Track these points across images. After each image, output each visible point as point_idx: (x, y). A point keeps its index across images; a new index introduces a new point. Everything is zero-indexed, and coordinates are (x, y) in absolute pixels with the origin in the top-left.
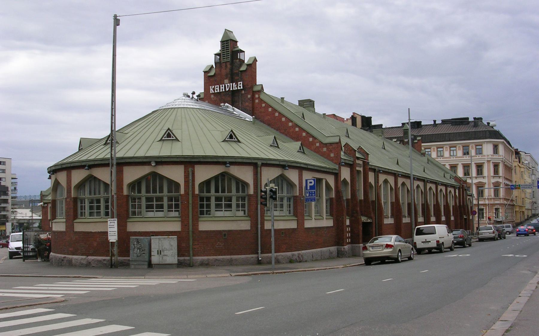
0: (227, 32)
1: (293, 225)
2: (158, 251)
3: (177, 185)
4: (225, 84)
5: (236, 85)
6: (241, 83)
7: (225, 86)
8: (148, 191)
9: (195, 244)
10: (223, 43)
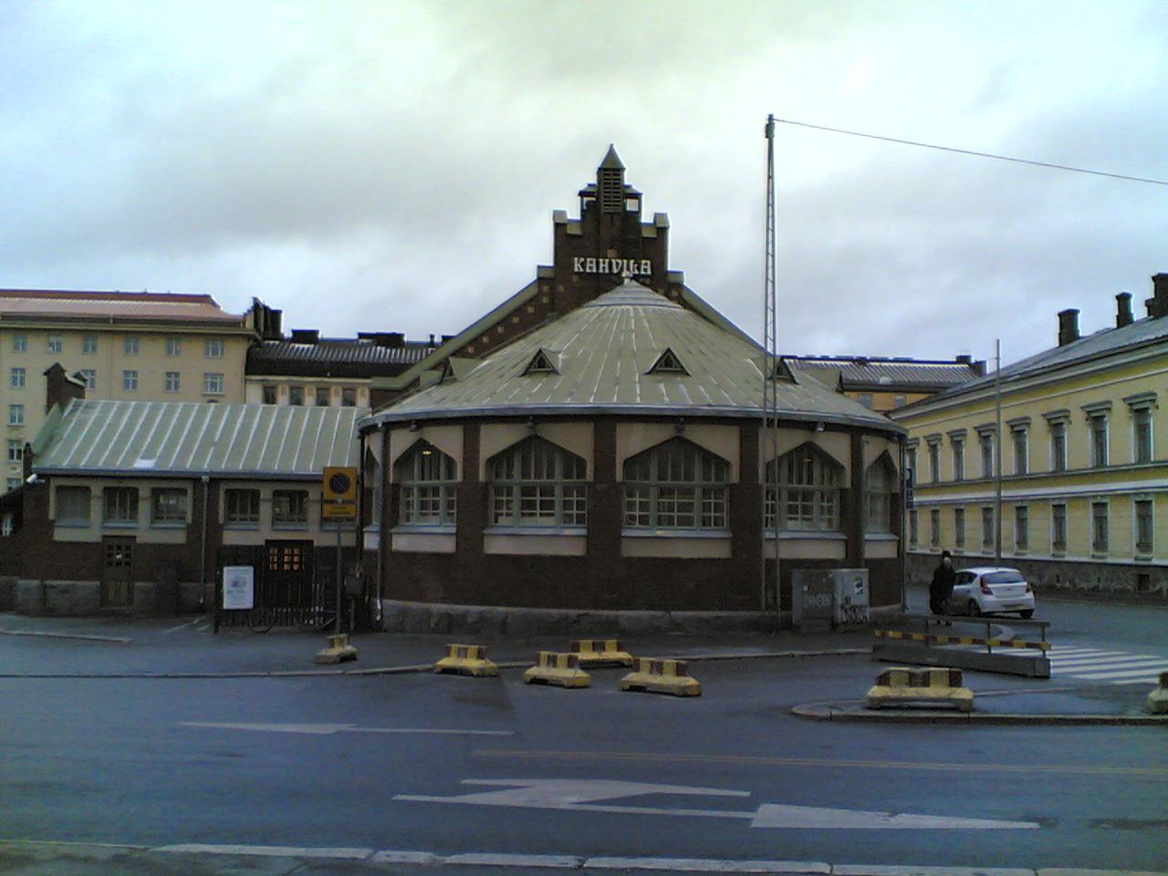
0: (611, 155)
3: (581, 463)
5: (636, 265)
6: (649, 262)
7: (610, 264)
8: (525, 475)
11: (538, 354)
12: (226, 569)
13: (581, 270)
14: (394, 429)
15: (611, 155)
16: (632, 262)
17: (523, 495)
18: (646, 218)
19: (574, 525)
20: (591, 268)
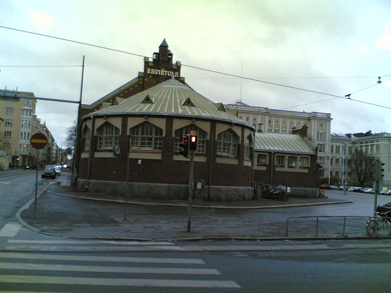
0: (164, 41)
1: (235, 162)
8: (142, 134)
11: (220, 110)
12: (174, 159)
13: (150, 73)
15: (164, 41)
16: (172, 72)
17: (155, 141)
18: (174, 61)
20: (153, 72)
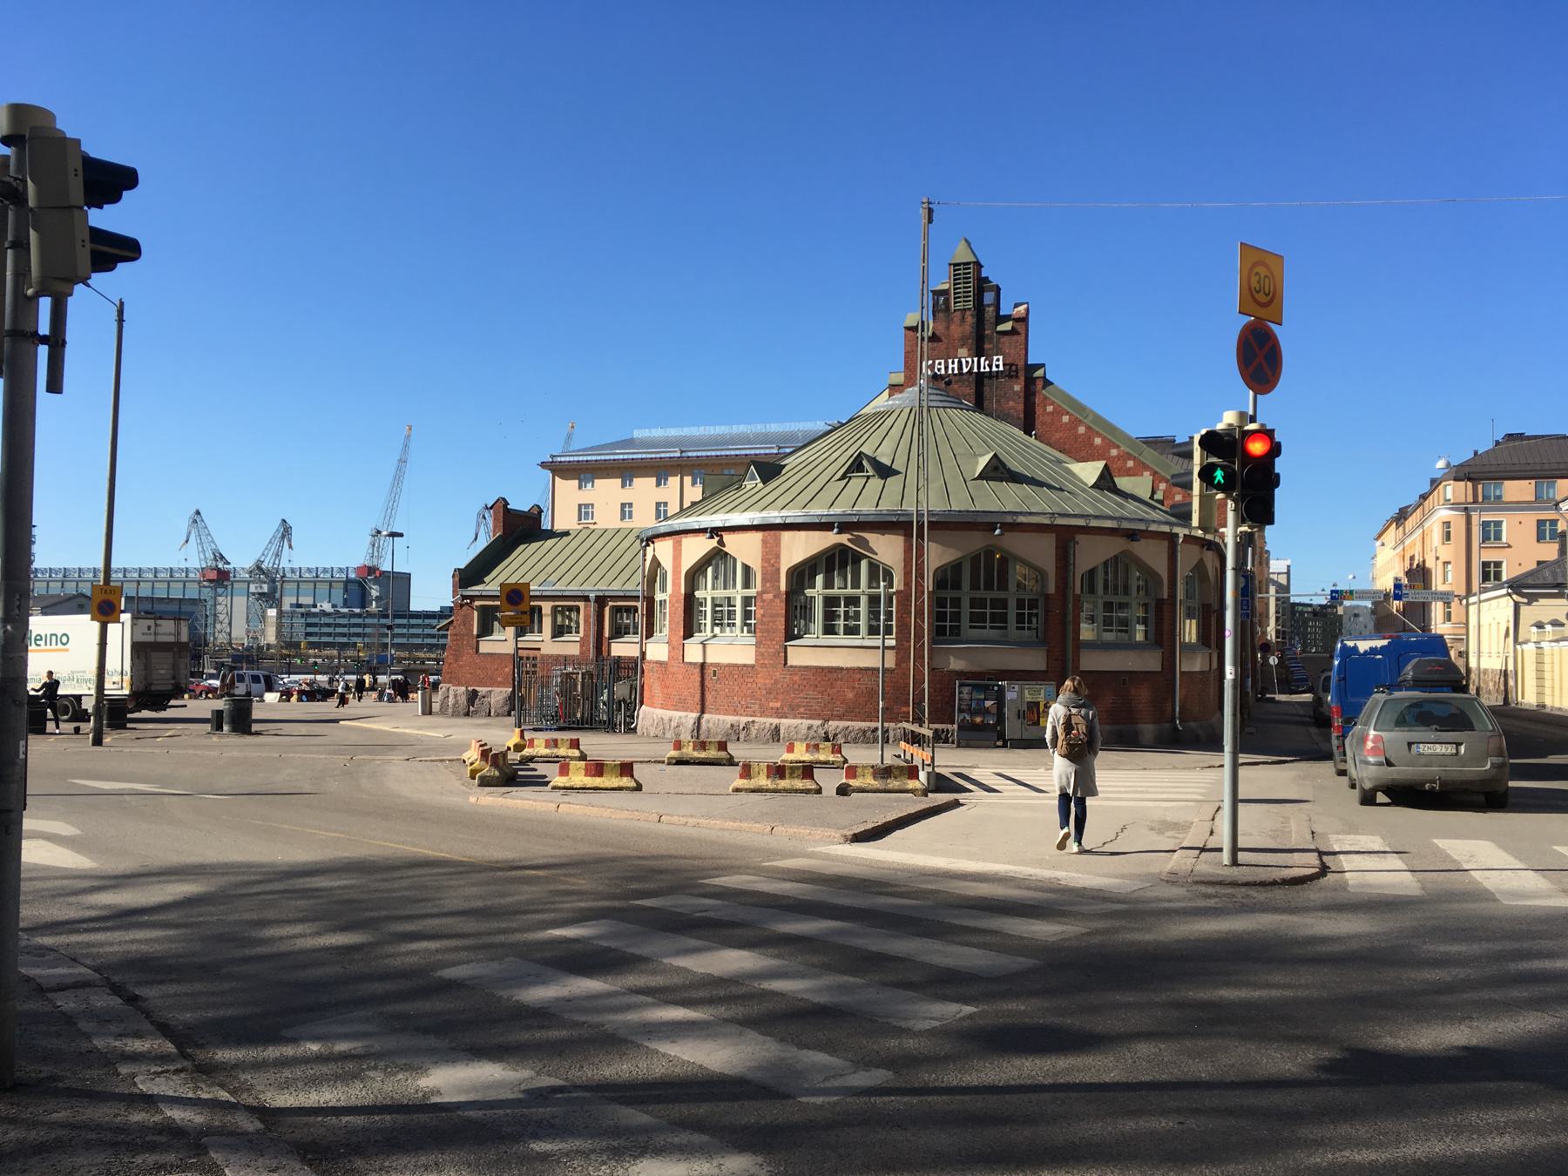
2: (1019, 711)
4: (960, 359)
5: (987, 362)
6: (1001, 357)
7: (960, 363)
9: (207, 683)
10: (957, 268)
14: (905, 542)
19: (947, 637)
